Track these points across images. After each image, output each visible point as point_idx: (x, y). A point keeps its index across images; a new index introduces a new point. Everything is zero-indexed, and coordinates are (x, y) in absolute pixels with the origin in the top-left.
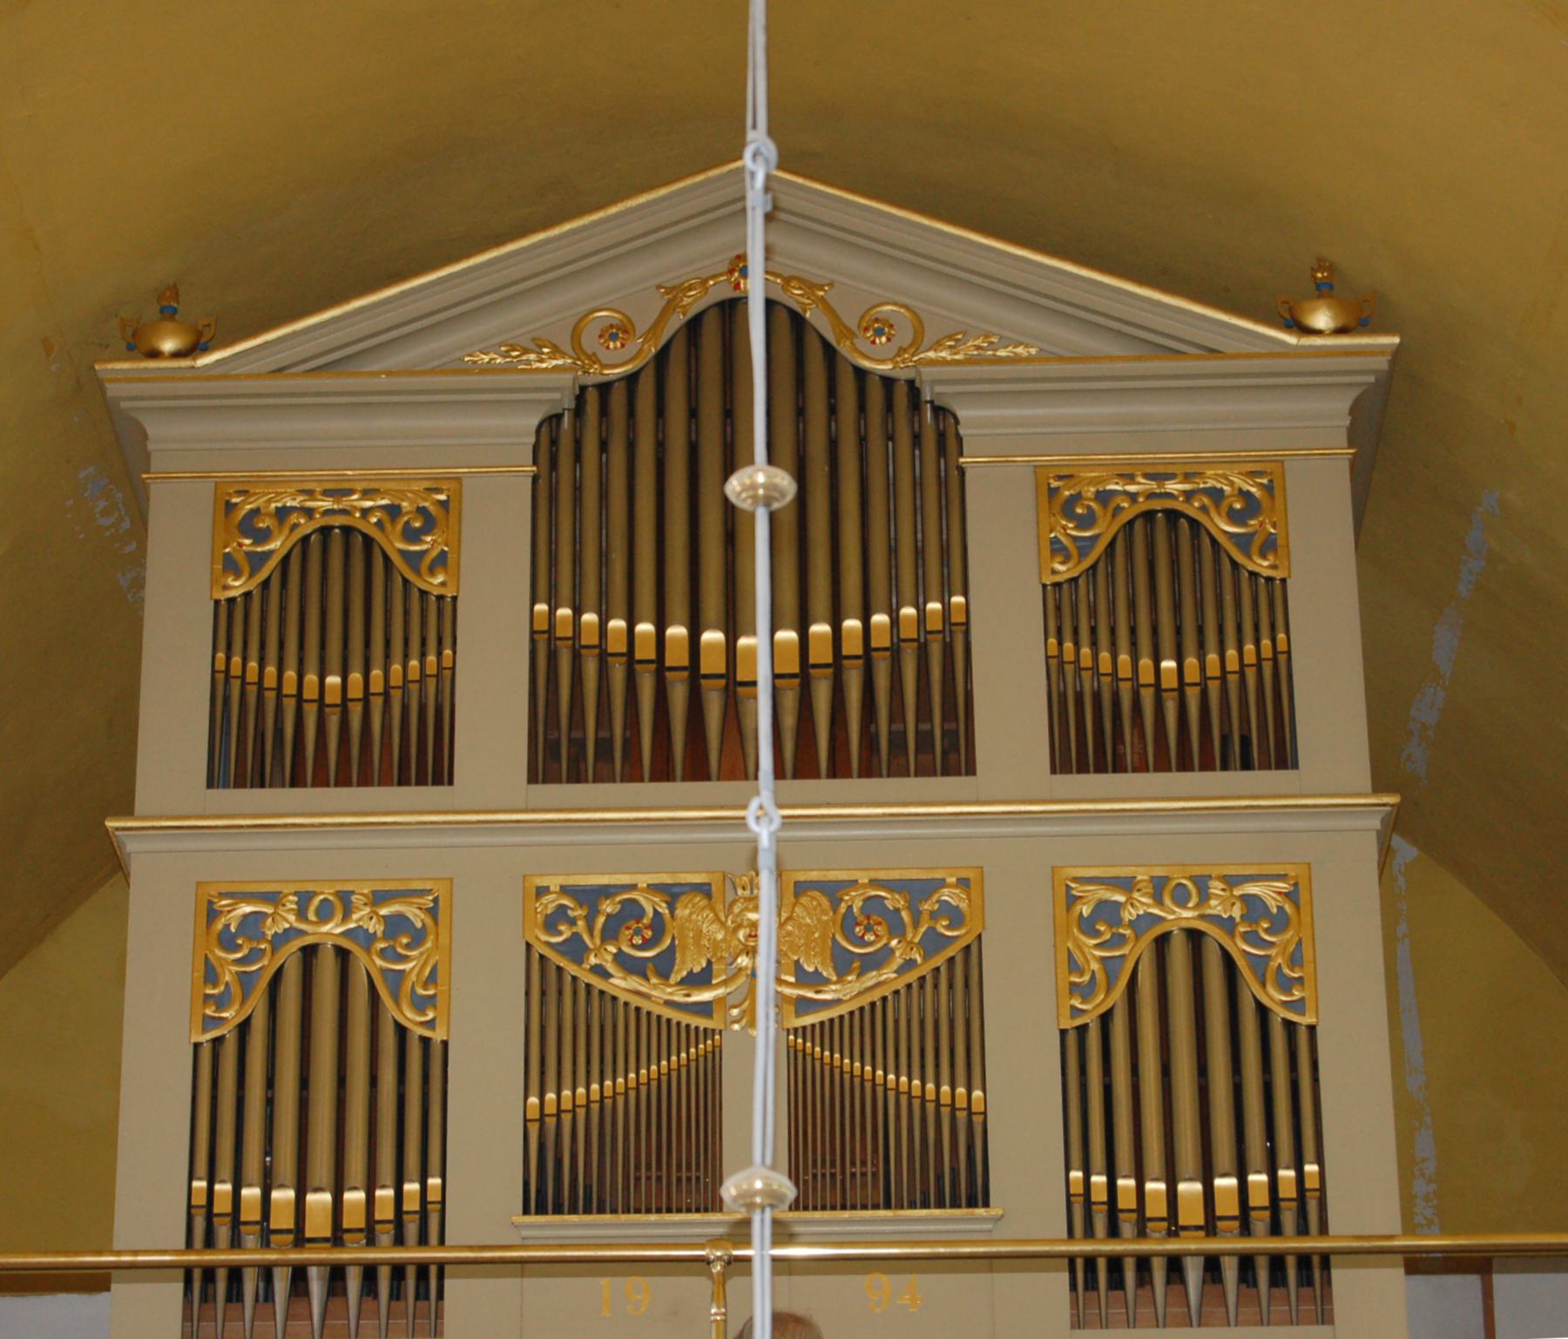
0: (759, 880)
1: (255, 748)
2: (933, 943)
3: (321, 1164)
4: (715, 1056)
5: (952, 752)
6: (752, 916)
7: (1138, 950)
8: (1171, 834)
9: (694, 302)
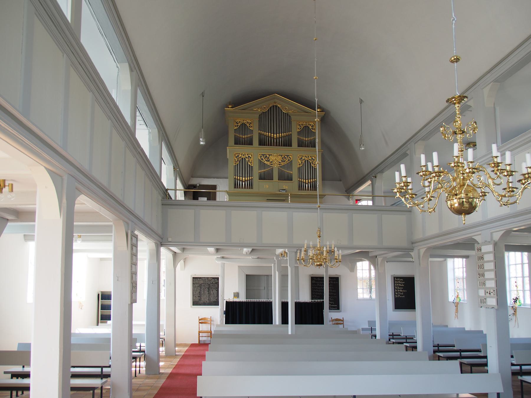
0: (275, 157)
1: (237, 142)
2: (289, 160)
3: (244, 176)
4: (272, 169)
5: (290, 145)
6: (223, 187)
7: (303, 161)
8: (305, 153)
9: (271, 105)
